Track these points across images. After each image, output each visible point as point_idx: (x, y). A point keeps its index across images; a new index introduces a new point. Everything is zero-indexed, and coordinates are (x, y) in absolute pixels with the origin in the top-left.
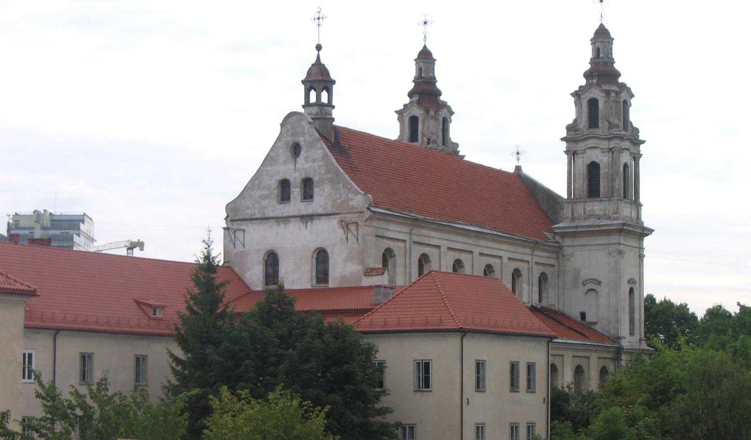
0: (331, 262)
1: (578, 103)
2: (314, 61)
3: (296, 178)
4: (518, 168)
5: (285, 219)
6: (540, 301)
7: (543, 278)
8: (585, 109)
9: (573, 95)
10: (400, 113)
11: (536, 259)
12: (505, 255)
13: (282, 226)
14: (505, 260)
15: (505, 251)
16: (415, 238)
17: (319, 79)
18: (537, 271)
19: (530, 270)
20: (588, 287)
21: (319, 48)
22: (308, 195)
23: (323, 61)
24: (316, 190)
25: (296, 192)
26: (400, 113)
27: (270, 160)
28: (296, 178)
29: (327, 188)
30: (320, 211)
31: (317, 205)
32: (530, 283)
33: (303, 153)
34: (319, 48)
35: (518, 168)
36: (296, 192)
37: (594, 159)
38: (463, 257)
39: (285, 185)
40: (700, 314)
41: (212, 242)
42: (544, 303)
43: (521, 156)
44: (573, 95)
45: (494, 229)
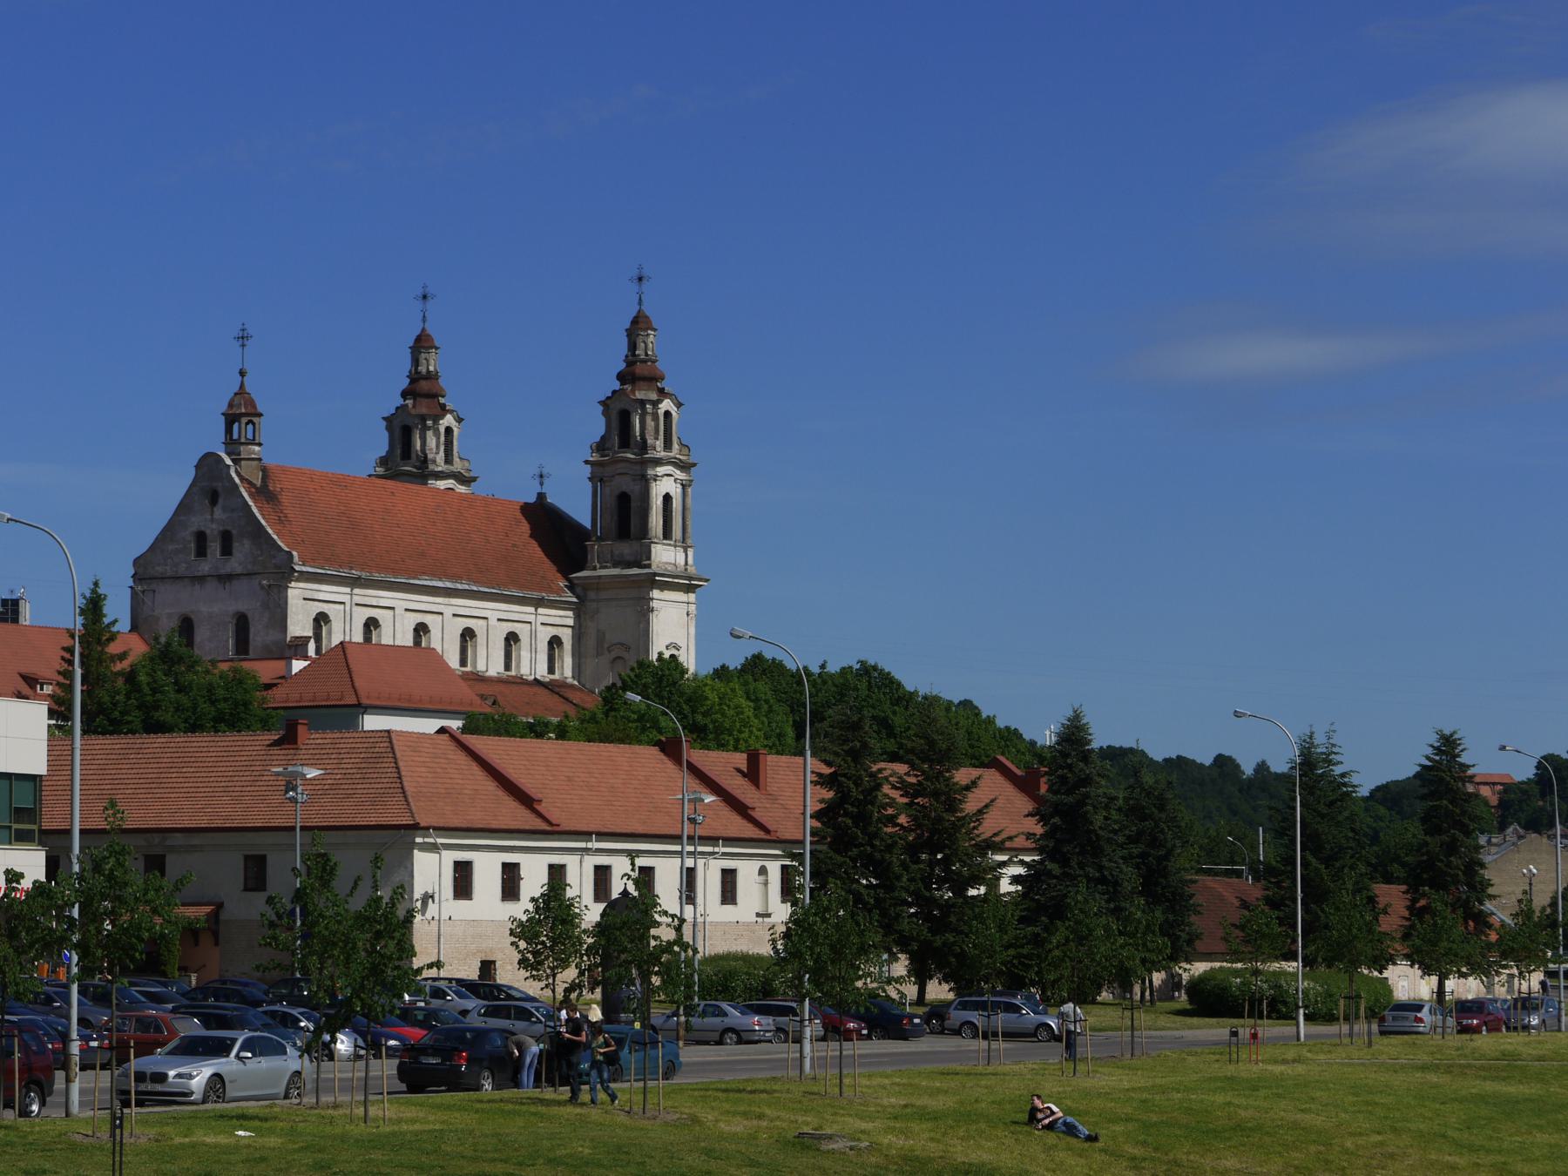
0: (252, 630)
1: (606, 413)
2: (236, 389)
3: (212, 530)
4: (541, 496)
5: (201, 579)
6: (551, 670)
7: (512, 639)
8: (615, 424)
9: (602, 403)
10: (389, 420)
11: (541, 619)
12: (448, 612)
13: (197, 587)
14: (493, 621)
15: (493, 610)
16: (357, 599)
17: (96, 584)
18: (545, 635)
19: (533, 635)
20: (614, 654)
21: (242, 373)
22: (227, 551)
23: (248, 389)
24: (236, 545)
25: (215, 548)
26: (389, 420)
27: (184, 507)
28: (212, 530)
29: (247, 543)
30: (239, 570)
31: (235, 564)
32: (534, 650)
33: (221, 501)
34: (242, 373)
35: (541, 496)
36: (215, 548)
37: (624, 489)
38: (427, 619)
39: (201, 538)
40: (984, 716)
41: (1069, 1041)
42: (556, 676)
43: (546, 481)
44: (602, 403)
45: (476, 582)
